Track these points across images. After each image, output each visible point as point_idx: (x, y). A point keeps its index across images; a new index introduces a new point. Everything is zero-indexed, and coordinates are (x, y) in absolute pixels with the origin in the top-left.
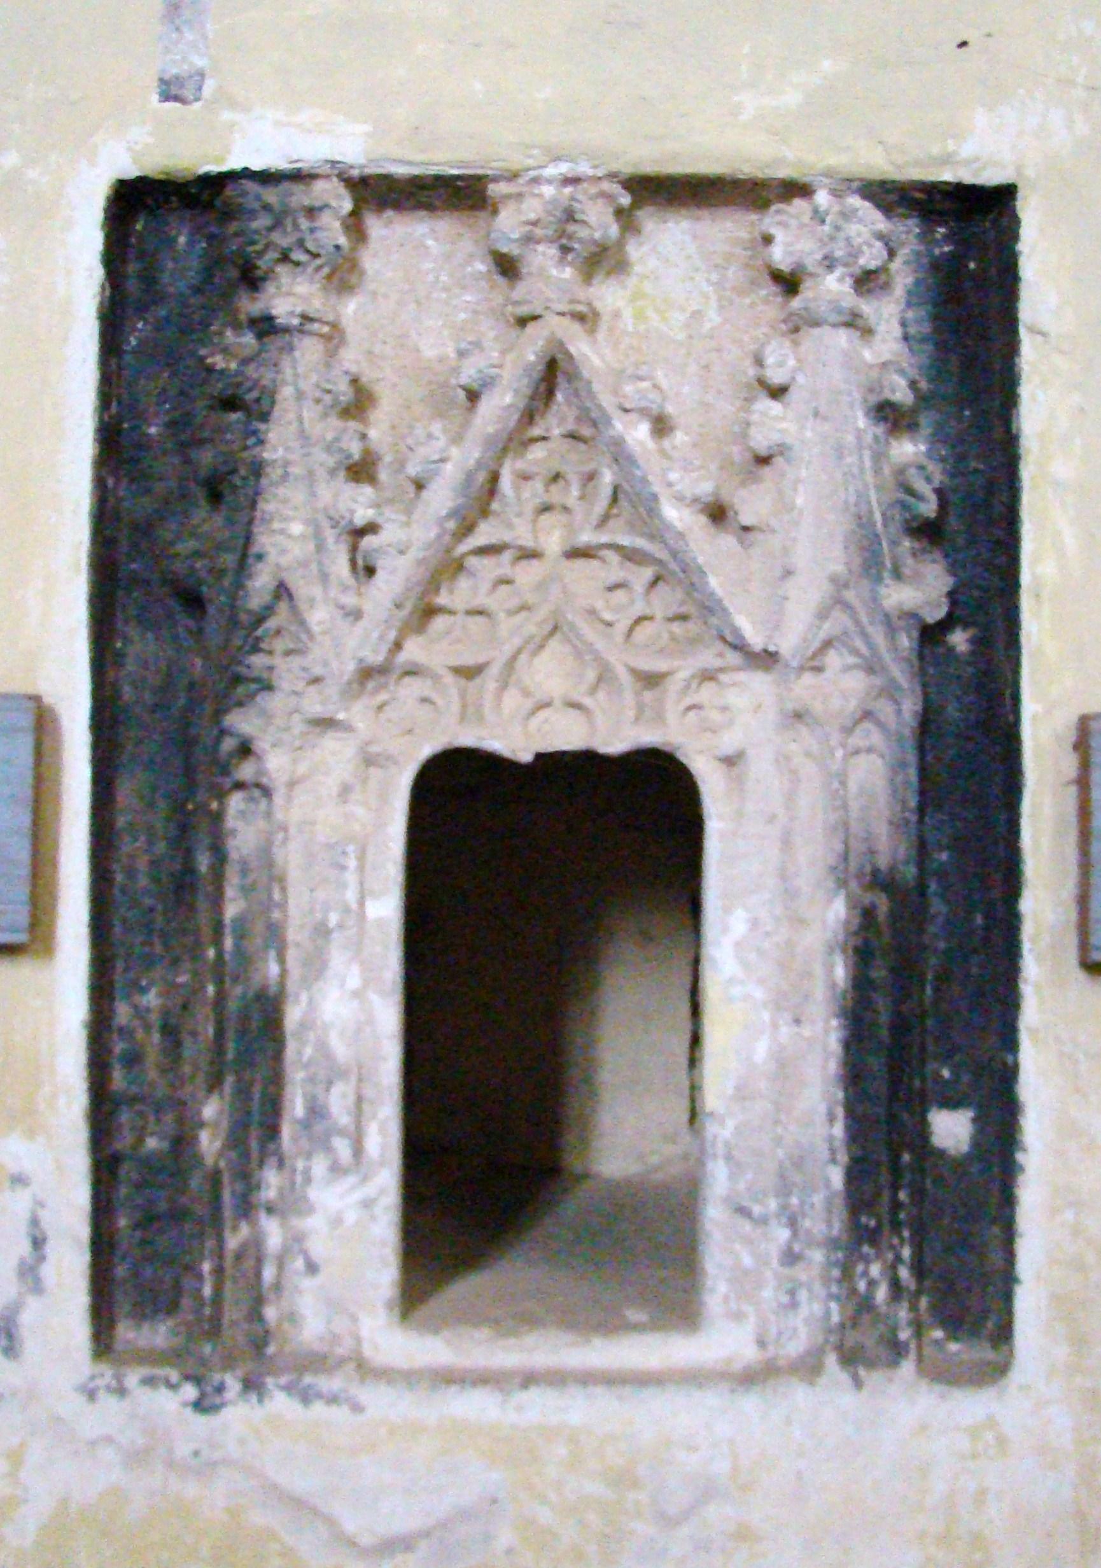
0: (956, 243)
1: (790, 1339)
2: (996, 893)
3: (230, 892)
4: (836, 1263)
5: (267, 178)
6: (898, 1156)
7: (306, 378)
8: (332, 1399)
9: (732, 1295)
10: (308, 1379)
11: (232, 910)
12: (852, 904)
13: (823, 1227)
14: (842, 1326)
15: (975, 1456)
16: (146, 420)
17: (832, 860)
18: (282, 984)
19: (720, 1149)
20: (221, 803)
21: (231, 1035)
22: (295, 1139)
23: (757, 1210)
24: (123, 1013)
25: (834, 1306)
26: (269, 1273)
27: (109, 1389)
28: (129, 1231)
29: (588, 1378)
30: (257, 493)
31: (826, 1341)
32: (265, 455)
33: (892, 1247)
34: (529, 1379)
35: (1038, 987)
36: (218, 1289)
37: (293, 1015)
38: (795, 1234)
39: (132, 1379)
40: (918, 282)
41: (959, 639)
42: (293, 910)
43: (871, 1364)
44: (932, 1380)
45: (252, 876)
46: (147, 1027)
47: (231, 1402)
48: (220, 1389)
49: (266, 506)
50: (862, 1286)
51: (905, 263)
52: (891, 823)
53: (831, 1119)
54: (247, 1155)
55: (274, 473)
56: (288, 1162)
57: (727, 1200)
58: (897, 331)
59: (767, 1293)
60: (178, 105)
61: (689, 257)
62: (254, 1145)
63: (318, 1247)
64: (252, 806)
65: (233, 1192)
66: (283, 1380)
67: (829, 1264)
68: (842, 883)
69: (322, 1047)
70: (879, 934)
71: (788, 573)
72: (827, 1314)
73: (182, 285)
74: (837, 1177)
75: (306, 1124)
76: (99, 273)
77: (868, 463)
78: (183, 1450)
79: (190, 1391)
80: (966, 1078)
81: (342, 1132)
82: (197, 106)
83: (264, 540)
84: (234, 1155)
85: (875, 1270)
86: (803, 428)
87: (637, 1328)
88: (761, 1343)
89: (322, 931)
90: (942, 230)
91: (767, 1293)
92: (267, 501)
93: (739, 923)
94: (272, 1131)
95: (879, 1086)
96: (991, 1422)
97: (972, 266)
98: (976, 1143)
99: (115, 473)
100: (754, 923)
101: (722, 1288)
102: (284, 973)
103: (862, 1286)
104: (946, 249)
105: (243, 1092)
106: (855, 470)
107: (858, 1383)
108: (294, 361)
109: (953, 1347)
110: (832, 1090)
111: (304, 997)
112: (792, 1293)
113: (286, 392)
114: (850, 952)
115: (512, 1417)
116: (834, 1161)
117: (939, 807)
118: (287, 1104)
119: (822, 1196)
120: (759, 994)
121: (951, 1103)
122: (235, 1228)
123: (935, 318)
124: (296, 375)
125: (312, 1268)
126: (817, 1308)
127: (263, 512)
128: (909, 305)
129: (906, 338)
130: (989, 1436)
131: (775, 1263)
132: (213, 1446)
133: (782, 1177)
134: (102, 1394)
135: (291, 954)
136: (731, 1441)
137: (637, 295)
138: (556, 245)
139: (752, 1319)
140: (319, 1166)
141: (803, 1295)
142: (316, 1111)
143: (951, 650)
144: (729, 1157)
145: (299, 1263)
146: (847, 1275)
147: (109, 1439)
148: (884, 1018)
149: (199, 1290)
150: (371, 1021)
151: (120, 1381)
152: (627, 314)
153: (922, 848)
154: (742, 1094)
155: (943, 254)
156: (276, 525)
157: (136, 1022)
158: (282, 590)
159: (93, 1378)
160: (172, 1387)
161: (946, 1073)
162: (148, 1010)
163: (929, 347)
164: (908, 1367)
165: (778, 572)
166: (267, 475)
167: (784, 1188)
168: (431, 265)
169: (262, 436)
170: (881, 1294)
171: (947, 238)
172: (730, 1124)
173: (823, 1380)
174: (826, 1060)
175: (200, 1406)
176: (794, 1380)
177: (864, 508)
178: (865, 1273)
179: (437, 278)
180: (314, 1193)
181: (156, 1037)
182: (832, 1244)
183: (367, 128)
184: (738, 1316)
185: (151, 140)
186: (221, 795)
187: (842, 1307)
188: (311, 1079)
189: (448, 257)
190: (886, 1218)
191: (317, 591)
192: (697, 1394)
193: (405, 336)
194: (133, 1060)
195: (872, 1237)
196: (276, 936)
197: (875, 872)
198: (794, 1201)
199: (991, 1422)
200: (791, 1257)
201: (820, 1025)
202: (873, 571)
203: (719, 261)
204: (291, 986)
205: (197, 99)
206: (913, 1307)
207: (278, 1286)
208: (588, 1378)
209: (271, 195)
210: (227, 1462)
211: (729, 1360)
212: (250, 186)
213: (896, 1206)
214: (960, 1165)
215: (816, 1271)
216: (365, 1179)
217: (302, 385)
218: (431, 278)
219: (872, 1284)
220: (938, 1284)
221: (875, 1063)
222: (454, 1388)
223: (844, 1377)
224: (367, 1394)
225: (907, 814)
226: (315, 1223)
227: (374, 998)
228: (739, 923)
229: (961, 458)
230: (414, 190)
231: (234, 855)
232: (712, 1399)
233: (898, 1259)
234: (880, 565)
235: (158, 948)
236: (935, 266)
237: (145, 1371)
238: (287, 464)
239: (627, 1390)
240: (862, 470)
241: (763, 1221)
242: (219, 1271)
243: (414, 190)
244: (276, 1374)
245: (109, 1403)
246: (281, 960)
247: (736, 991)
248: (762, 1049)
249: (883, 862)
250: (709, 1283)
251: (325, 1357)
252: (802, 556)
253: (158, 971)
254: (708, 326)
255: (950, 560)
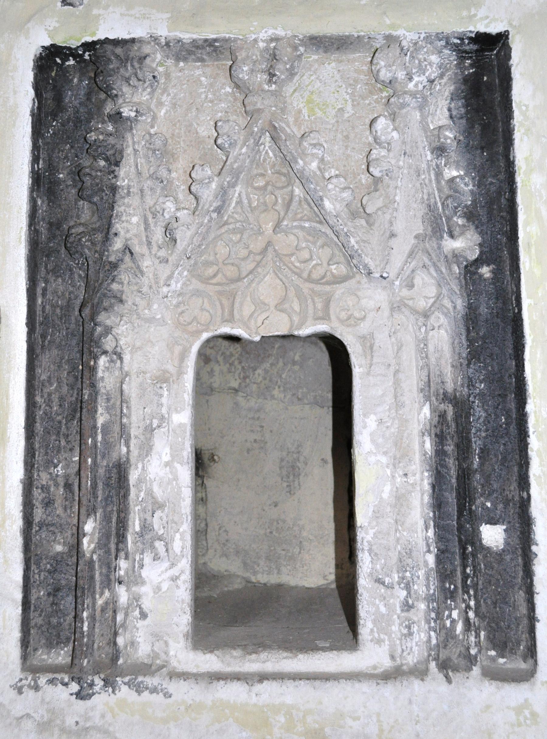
0: (477, 67)
1: (409, 654)
2: (513, 406)
3: (100, 410)
4: (433, 610)
5: (116, 42)
6: (464, 549)
7: (139, 143)
8: (154, 690)
9: (375, 629)
10: (140, 679)
11: (101, 420)
12: (433, 410)
13: (424, 588)
14: (438, 645)
15: (519, 725)
16: (58, 171)
17: (421, 384)
18: (128, 459)
19: (366, 546)
20: (95, 362)
21: (100, 486)
22: (135, 543)
23: (387, 580)
24: (44, 478)
25: (432, 634)
26: (120, 618)
27: (29, 686)
28: (46, 597)
29: (296, 677)
30: (114, 202)
31: (430, 655)
32: (118, 183)
33: (464, 601)
34: (263, 677)
35: (539, 455)
36: (92, 627)
37: (133, 476)
38: (409, 593)
39: (43, 680)
40: (456, 89)
41: (486, 271)
42: (134, 418)
43: (456, 669)
44: (492, 679)
45: (112, 402)
46: (57, 485)
47: (97, 692)
48: (92, 685)
49: (119, 209)
50: (448, 623)
51: (449, 79)
52: (453, 366)
53: (427, 529)
54: (108, 552)
55: (122, 192)
56: (130, 557)
57: (371, 574)
58: (447, 113)
59: (395, 628)
60: (71, 7)
61: (336, 81)
62: (113, 546)
63: (147, 604)
64: (112, 364)
65: (101, 573)
66: (126, 679)
67: (429, 610)
68: (427, 398)
69: (150, 493)
70: (448, 427)
71: (393, 235)
72: (430, 637)
73: (76, 103)
74: (431, 559)
75: (141, 535)
76: (32, 93)
77: (433, 177)
78: (70, 721)
79: (74, 687)
80: (500, 506)
81: (160, 539)
82: (81, 7)
83: (118, 226)
84: (101, 552)
85: (455, 614)
86: (398, 160)
87: (324, 649)
88: (393, 657)
89: (150, 430)
90: (469, 61)
91: (395, 628)
92: (119, 206)
93: (372, 422)
94: (121, 538)
95: (452, 508)
96: (526, 704)
97: (485, 78)
98: (507, 543)
99: (38, 190)
100: (381, 422)
101: (370, 625)
102: (128, 452)
103: (448, 623)
104: (471, 71)
105: (107, 518)
106: (427, 181)
107: (449, 680)
108: (133, 135)
109: (502, 661)
110: (427, 511)
111: (140, 466)
112: (409, 627)
113: (129, 150)
114: (433, 436)
115: (254, 699)
116: (429, 551)
117: (479, 360)
118: (130, 523)
119: (423, 571)
120: (384, 460)
121: (492, 522)
122: (102, 594)
123: (466, 106)
124: (134, 143)
125: (144, 615)
126: (423, 636)
127: (118, 212)
128: (452, 99)
129: (451, 117)
130: (527, 712)
131: (399, 611)
132: (87, 719)
133: (400, 560)
134: (25, 689)
135: (133, 442)
136: (378, 715)
137: (309, 101)
138: (267, 73)
139: (387, 642)
140: (147, 558)
141: (415, 629)
142: (146, 527)
143: (481, 276)
144: (370, 551)
145: (137, 613)
146: (439, 617)
147: (28, 715)
148: (453, 472)
149: (82, 628)
150: (176, 478)
151: (36, 682)
152: (305, 112)
153: (471, 384)
154: (377, 515)
155: (469, 73)
156: (124, 218)
157: (51, 483)
158: (127, 251)
159: (21, 680)
160: (66, 685)
161: (489, 504)
162: (57, 476)
163: (464, 121)
164: (476, 670)
165: (387, 234)
166: (119, 193)
167: (402, 569)
168: (203, 90)
169: (116, 174)
170: (459, 627)
171: (472, 66)
172: (371, 532)
173: (428, 679)
174: (422, 495)
175: (79, 695)
176: (412, 678)
177: (432, 201)
178: (450, 616)
179: (206, 97)
180: (145, 573)
181: (61, 491)
182: (429, 599)
183: (168, 15)
184: (379, 642)
185: (57, 25)
186: (96, 358)
187: (438, 635)
188: (144, 510)
189: (211, 85)
190: (459, 585)
191: (145, 250)
192: (357, 685)
193: (191, 125)
194: (48, 503)
195: (452, 595)
196: (124, 432)
197: (445, 394)
198: (408, 574)
199: (526, 704)
200: (407, 607)
201: (418, 476)
202: (438, 234)
203: (352, 82)
204: (133, 460)
205: (81, 5)
206: (477, 636)
207: (123, 625)
208: (296, 677)
209: (119, 51)
210: (93, 728)
211: (375, 667)
212: (109, 47)
213: (465, 577)
214: (500, 555)
215: (421, 615)
216: (173, 565)
217: (136, 147)
218: (203, 96)
219: (453, 622)
220: (276, 346)
221: (451, 498)
222: (222, 682)
223: (441, 676)
224: (173, 687)
225: (461, 360)
226: (145, 590)
227: (177, 466)
228: (372, 422)
229: (483, 177)
230: (193, 49)
231: (103, 391)
232: (365, 687)
233: (468, 607)
234: (441, 230)
235: (63, 443)
236: (466, 80)
237: (50, 676)
238: (129, 187)
239: (317, 683)
240: (430, 181)
241: (390, 587)
242: (92, 618)
243: (193, 49)
244: (122, 675)
245: (30, 694)
246: (128, 446)
247: (372, 459)
248: (387, 491)
249: (450, 387)
250: (362, 622)
251: (151, 666)
252: (399, 227)
253: (63, 455)
254: (346, 115)
255: (479, 230)
